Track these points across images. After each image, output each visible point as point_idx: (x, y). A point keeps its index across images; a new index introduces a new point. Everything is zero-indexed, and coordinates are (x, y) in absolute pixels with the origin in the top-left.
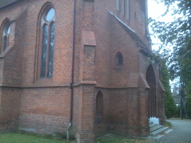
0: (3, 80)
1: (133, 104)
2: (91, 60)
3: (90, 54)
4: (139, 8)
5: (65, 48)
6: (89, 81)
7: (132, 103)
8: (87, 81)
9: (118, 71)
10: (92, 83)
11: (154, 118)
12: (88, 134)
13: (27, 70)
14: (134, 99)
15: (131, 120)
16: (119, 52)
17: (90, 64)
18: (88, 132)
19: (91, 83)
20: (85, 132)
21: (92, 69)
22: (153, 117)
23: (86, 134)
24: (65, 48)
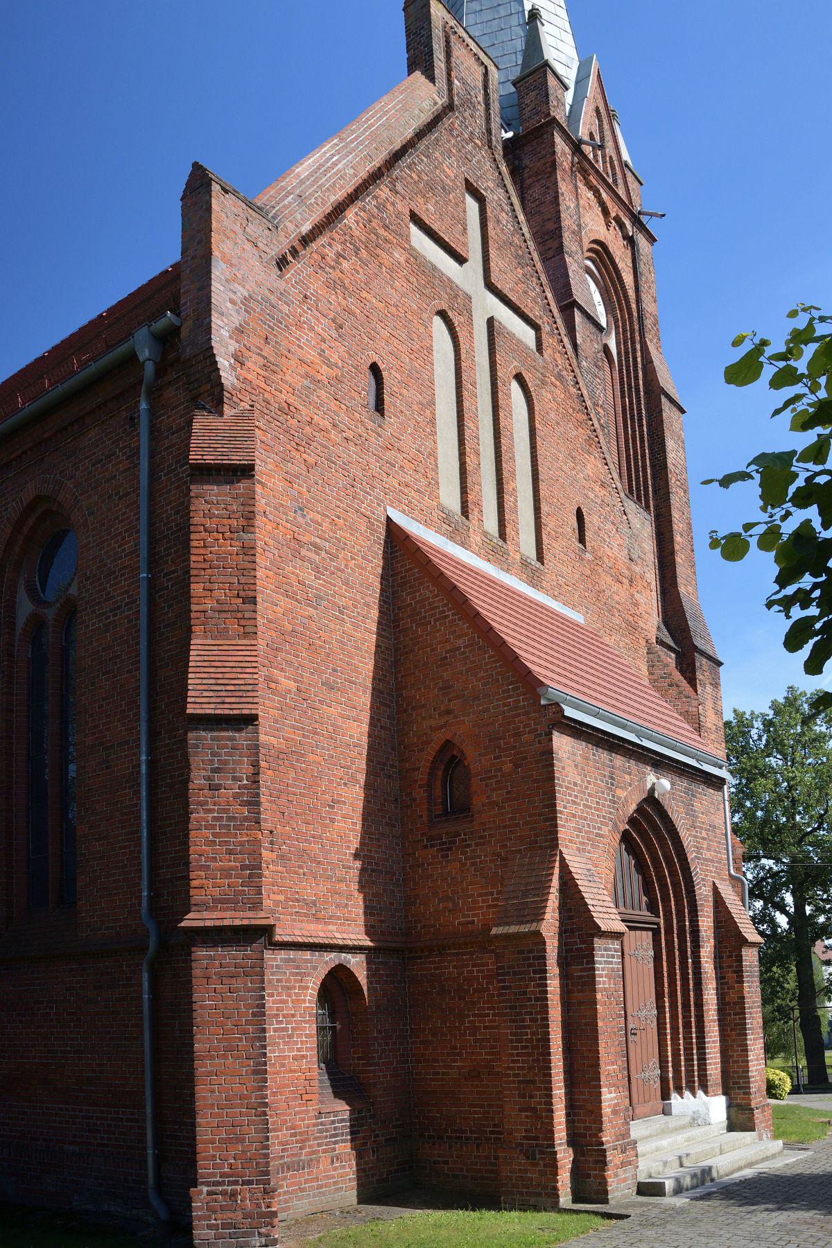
0: (192, 961)
1: (529, 1027)
2: (235, 796)
3: (226, 762)
4: (603, 485)
5: (127, 742)
6: (228, 914)
7: (523, 1020)
8: (215, 915)
9: (450, 849)
10: (246, 922)
11: (681, 1095)
12: (234, 1195)
13: (358, 864)
14: (530, 999)
15: (521, 1110)
16: (448, 744)
17: (229, 819)
18: (236, 1183)
19: (238, 922)
20: (222, 1184)
21: (242, 844)
22: (687, 1094)
23: (224, 1193)
24: (127, 742)
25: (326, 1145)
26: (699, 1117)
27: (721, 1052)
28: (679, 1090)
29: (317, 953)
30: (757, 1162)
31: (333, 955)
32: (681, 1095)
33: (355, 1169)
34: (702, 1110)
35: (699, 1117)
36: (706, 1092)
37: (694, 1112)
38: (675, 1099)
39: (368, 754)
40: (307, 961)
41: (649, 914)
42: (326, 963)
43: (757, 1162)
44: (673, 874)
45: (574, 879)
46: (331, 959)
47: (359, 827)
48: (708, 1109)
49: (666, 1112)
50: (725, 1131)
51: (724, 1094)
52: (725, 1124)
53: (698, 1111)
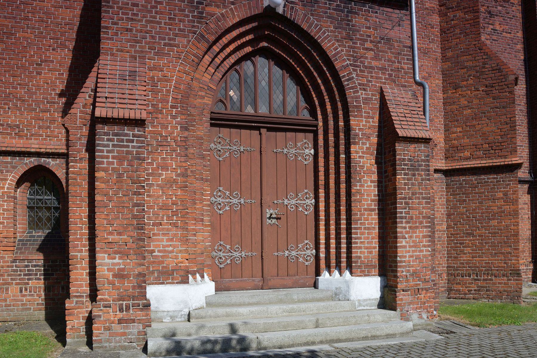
22: (336, 273)
25: (19, 280)
26: (341, 293)
27: (380, 238)
28: (328, 268)
29: (18, 158)
30: (339, 341)
31: (32, 159)
32: (330, 273)
33: (43, 297)
34: (343, 287)
35: (341, 293)
36: (351, 273)
37: (337, 289)
38: (325, 276)
39: (79, 28)
40: (7, 163)
41: (311, 118)
42: (26, 164)
43: (339, 341)
44: (326, 82)
45: (392, 120)
46: (30, 162)
47: (65, 76)
48: (348, 287)
49: (315, 286)
50: (376, 307)
51: (380, 275)
52: (377, 302)
53: (340, 288)
